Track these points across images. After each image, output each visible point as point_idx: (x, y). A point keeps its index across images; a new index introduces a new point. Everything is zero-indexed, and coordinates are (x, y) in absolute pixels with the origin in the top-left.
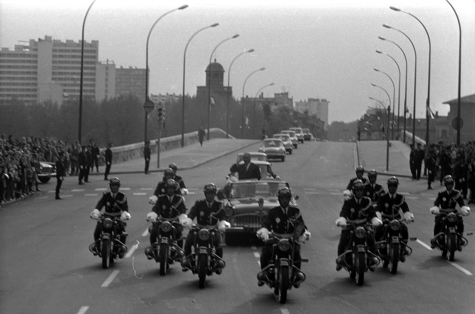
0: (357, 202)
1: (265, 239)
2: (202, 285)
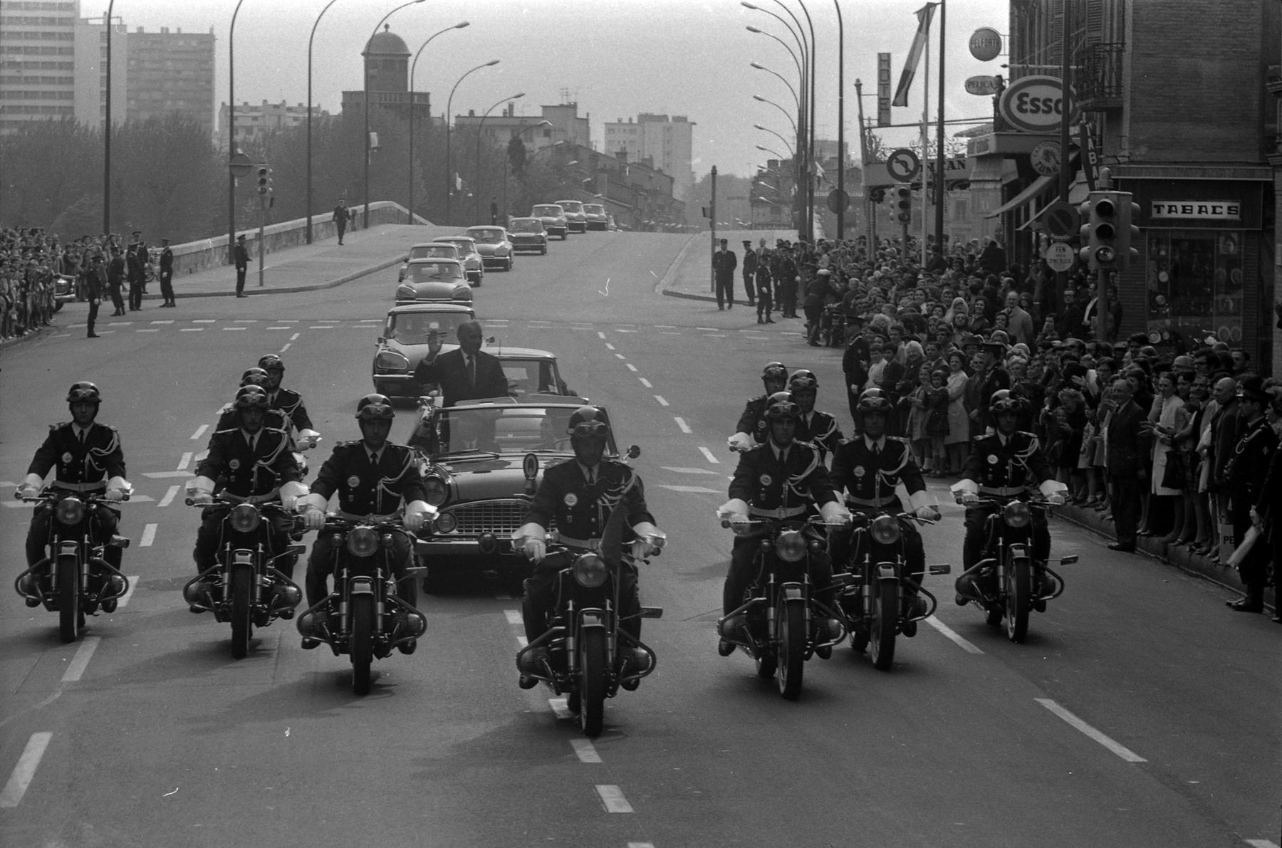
0: (777, 456)
1: (537, 556)
2: (360, 685)
